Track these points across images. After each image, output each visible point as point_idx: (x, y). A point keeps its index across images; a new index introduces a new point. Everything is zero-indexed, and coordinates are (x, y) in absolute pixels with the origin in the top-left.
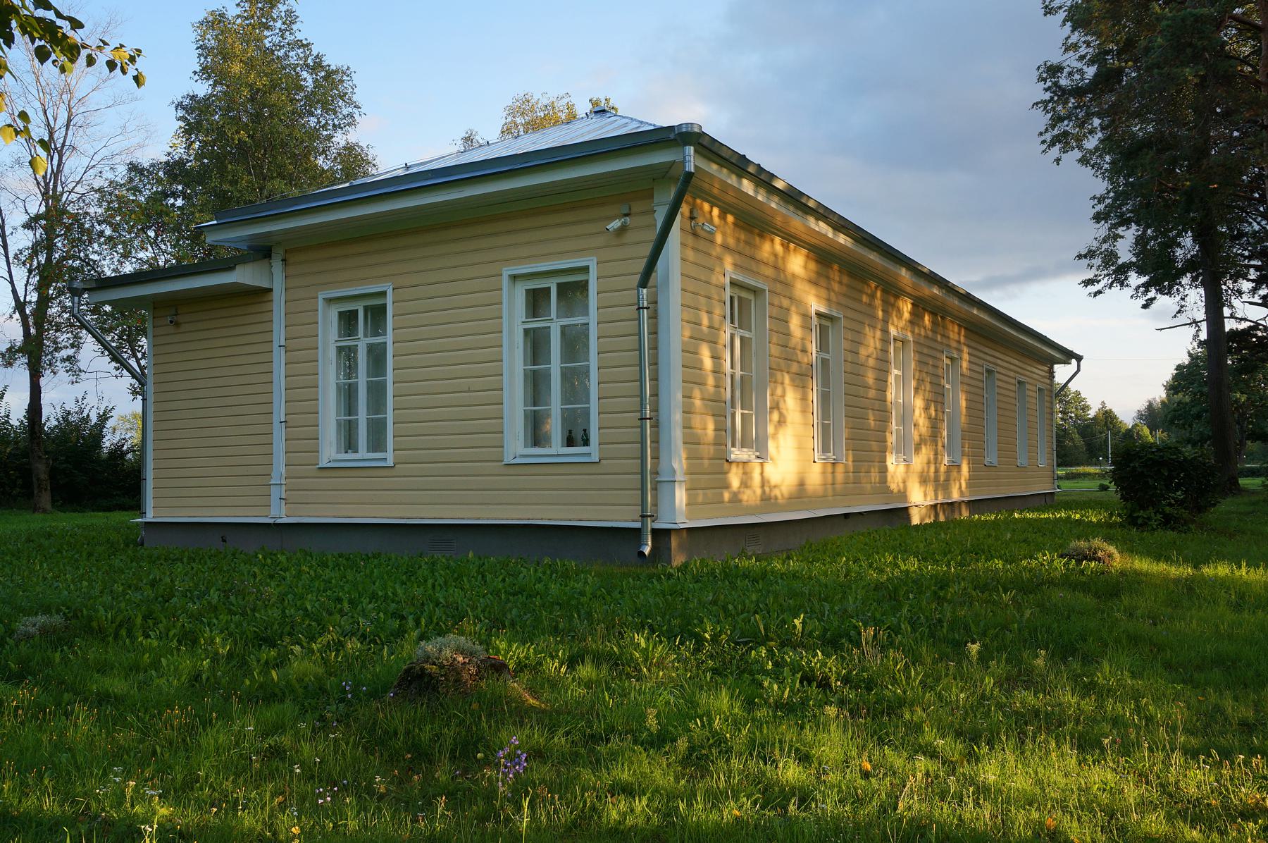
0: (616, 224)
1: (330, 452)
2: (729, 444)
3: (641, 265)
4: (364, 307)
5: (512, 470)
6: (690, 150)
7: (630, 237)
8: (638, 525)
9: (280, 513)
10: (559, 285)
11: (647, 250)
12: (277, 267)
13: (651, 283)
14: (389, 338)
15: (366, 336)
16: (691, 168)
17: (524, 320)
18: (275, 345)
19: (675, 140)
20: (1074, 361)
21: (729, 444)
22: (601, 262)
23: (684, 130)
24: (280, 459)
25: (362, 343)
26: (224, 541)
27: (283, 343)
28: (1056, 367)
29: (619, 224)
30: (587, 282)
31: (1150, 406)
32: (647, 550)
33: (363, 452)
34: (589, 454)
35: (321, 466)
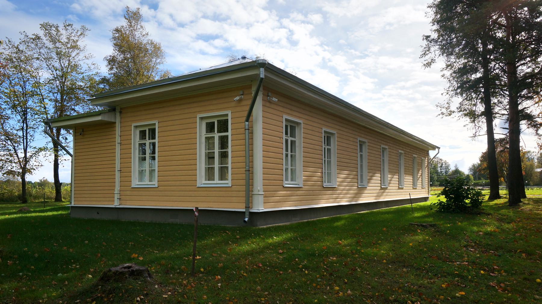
0: (237, 98)
1: (135, 183)
2: (284, 179)
3: (246, 113)
4: (149, 129)
5: (200, 189)
6: (262, 70)
7: (244, 103)
8: (244, 210)
9: (116, 204)
10: (218, 121)
11: (248, 108)
12: (118, 115)
13: (250, 120)
14: (229, 134)
15: (149, 139)
16: (262, 76)
17: (205, 133)
18: (117, 142)
19: (257, 66)
20: (437, 149)
21: (284, 179)
22: (233, 112)
23: (260, 62)
24: (117, 184)
25: (216, 135)
26: (98, 213)
27: (119, 142)
28: (430, 151)
29: (239, 98)
30: (228, 119)
31: (474, 166)
32: (246, 219)
33: (147, 182)
34: (228, 184)
35: (132, 187)
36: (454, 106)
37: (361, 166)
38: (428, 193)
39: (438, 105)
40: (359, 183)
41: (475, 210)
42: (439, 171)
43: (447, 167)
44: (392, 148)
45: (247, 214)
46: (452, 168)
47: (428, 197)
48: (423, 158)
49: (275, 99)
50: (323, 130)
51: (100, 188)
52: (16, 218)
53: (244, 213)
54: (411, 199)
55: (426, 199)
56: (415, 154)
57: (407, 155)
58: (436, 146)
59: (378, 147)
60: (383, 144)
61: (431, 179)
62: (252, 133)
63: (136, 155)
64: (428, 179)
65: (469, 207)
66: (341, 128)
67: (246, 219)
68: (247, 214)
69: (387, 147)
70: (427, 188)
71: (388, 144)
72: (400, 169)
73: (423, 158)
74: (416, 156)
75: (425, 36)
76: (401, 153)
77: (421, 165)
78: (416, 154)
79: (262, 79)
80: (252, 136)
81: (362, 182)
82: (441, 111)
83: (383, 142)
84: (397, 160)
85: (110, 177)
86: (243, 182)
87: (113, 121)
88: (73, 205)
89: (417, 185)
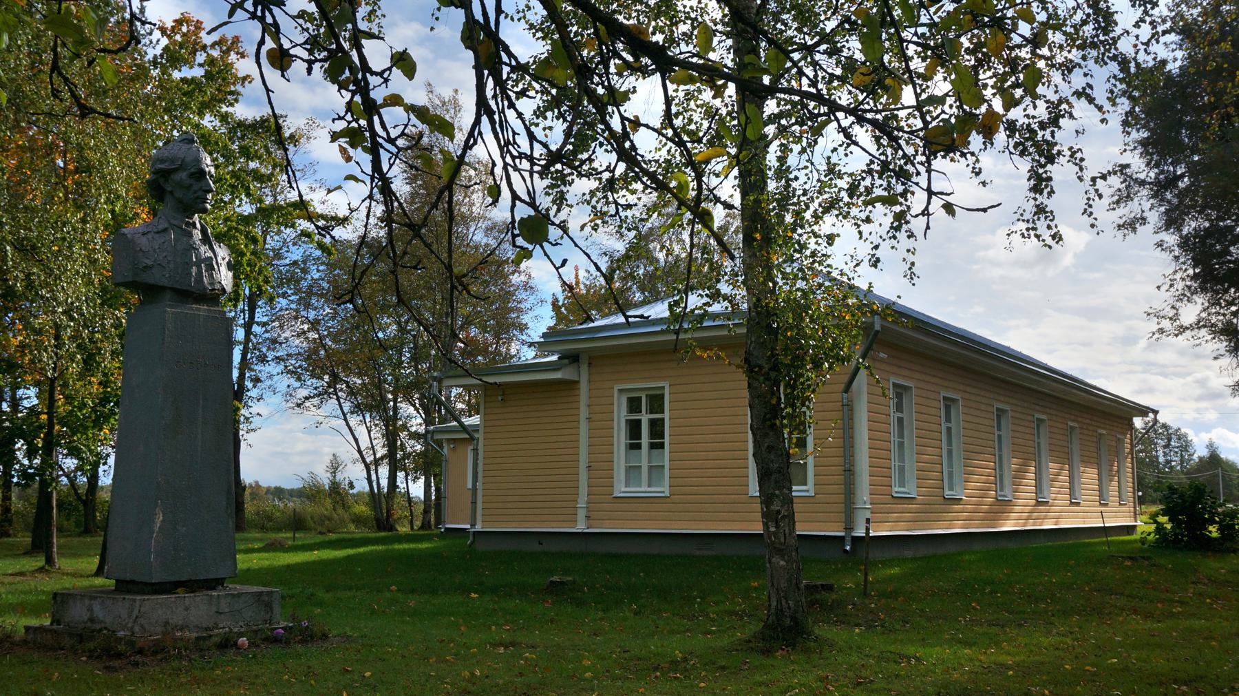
8: (842, 534)
9: (581, 527)
12: (584, 369)
20: (1151, 415)
32: (848, 548)
34: (808, 491)
36: (1191, 312)
37: (950, 452)
38: (1135, 518)
39: (1150, 311)
40: (999, 493)
41: (1228, 544)
42: (1161, 459)
43: (1185, 446)
44: (1054, 418)
45: (848, 540)
46: (1200, 452)
47: (1135, 526)
48: (1119, 436)
49: (882, 355)
50: (942, 395)
51: (541, 498)
52: (364, 553)
53: (842, 538)
54: (1104, 528)
55: (1130, 529)
56: (1100, 428)
57: (1086, 432)
58: (1148, 408)
59: (1030, 418)
60: (1038, 411)
61: (1140, 483)
62: (852, 410)
63: (621, 437)
64: (1133, 483)
65: (1215, 539)
66: (968, 389)
67: (848, 548)
68: (848, 540)
69: (1044, 417)
70: (1132, 504)
71: (1048, 410)
72: (1039, 457)
73: (1119, 436)
74: (1104, 432)
75: (1120, 166)
76: (1072, 427)
77: (1117, 451)
78: (1104, 428)
79: (878, 332)
80: (852, 414)
81: (1002, 490)
82: (1160, 326)
83: (1037, 407)
84: (1065, 444)
85: (568, 477)
86: (841, 488)
87: (576, 378)
88: (478, 528)
89: (1109, 496)
